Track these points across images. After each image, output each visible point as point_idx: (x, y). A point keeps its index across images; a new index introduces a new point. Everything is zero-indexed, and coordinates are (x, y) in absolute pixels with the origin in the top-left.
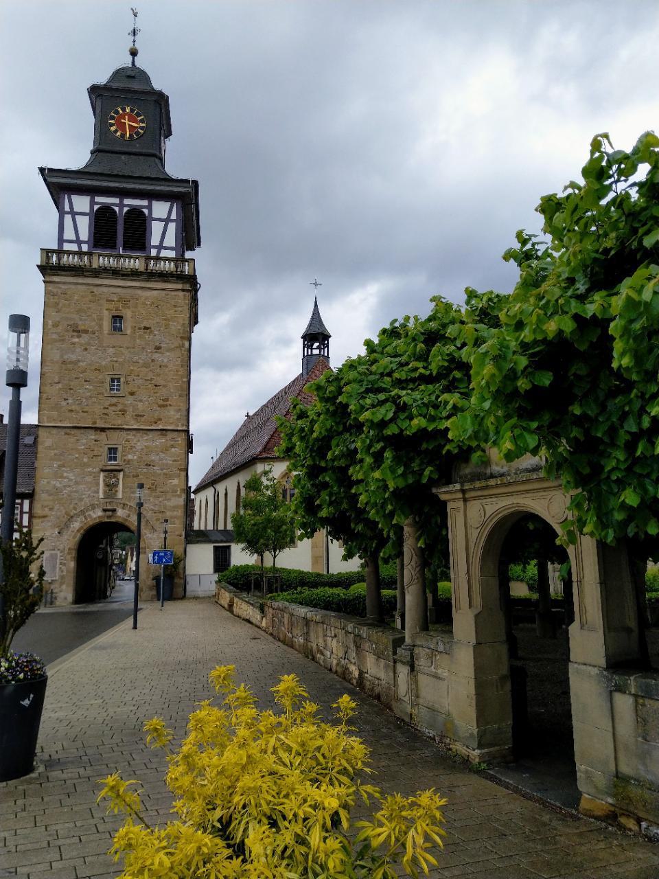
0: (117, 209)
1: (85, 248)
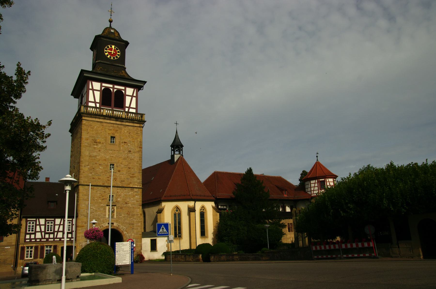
0: (112, 89)
1: (98, 105)
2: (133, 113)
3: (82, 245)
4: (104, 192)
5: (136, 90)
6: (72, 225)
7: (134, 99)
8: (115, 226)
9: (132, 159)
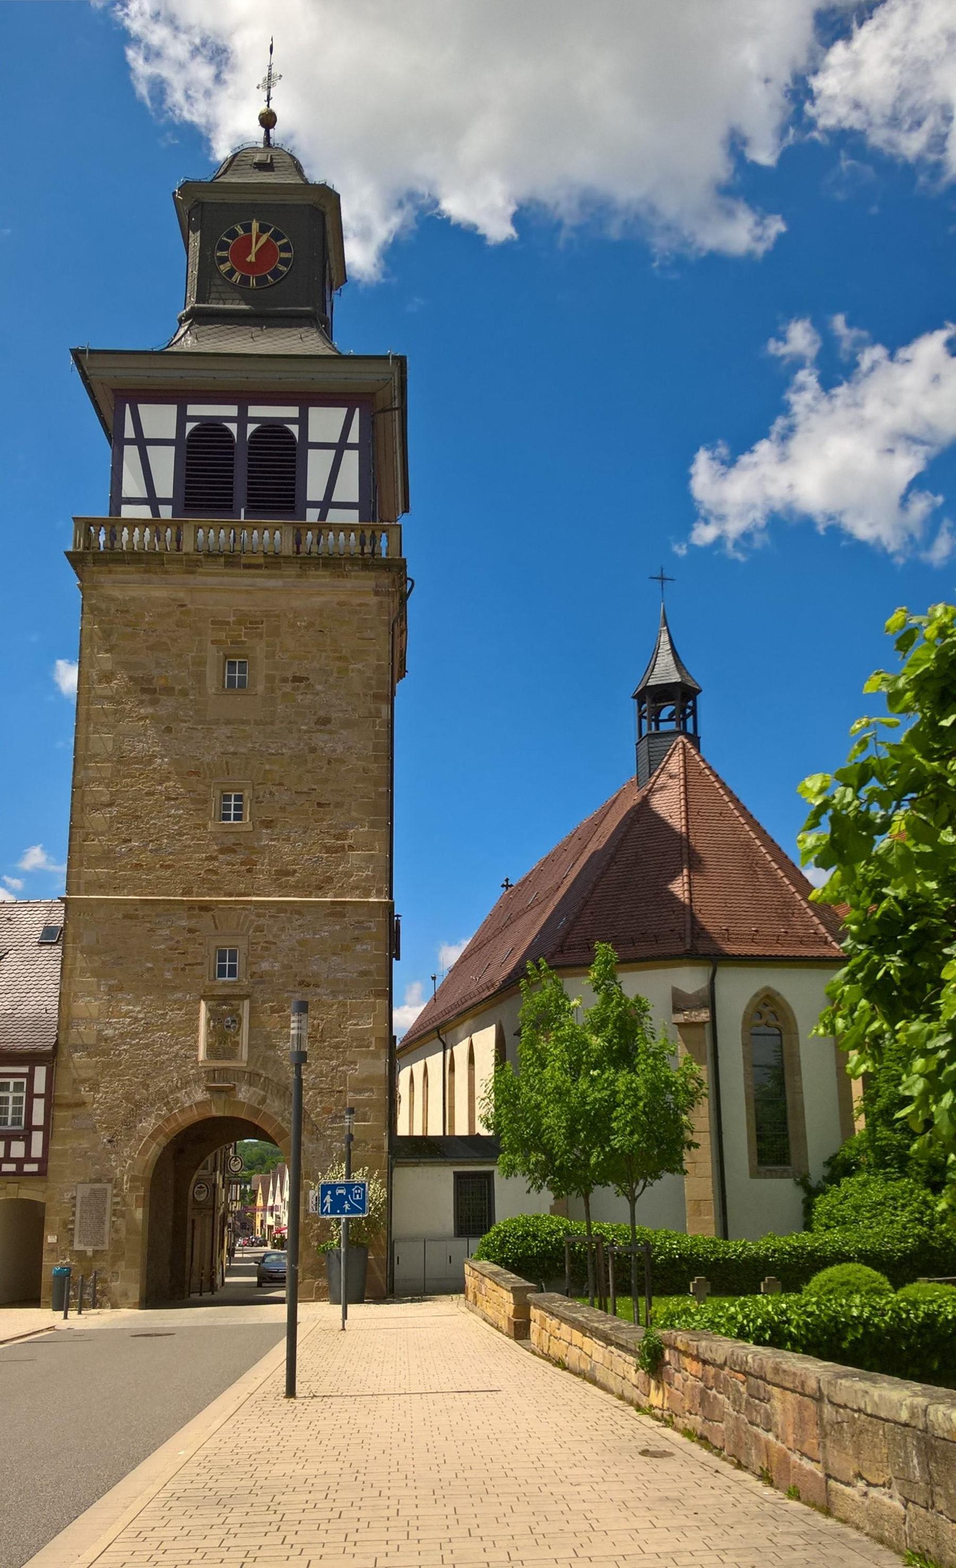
0: (233, 428)
1: (166, 512)
2: (347, 528)
3: (74, 1198)
4: (191, 931)
5: (357, 410)
6: (31, 1096)
7: (351, 459)
8: (244, 1103)
9: (336, 760)
